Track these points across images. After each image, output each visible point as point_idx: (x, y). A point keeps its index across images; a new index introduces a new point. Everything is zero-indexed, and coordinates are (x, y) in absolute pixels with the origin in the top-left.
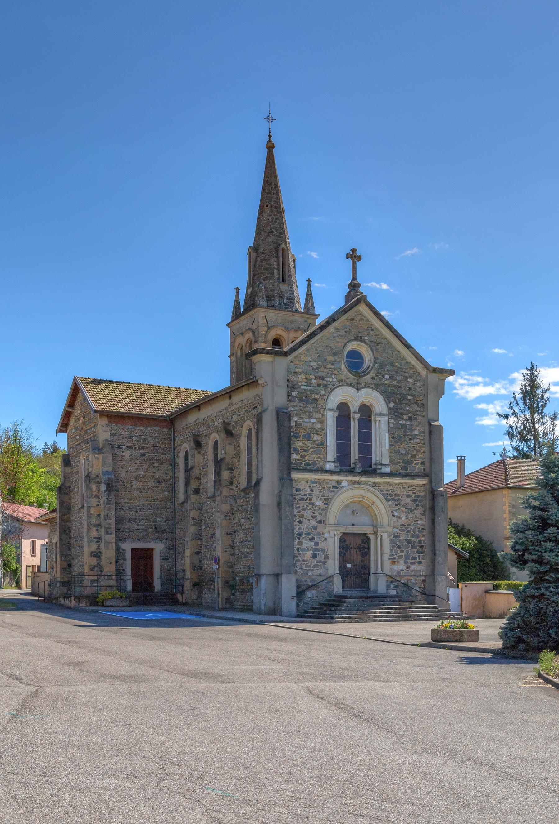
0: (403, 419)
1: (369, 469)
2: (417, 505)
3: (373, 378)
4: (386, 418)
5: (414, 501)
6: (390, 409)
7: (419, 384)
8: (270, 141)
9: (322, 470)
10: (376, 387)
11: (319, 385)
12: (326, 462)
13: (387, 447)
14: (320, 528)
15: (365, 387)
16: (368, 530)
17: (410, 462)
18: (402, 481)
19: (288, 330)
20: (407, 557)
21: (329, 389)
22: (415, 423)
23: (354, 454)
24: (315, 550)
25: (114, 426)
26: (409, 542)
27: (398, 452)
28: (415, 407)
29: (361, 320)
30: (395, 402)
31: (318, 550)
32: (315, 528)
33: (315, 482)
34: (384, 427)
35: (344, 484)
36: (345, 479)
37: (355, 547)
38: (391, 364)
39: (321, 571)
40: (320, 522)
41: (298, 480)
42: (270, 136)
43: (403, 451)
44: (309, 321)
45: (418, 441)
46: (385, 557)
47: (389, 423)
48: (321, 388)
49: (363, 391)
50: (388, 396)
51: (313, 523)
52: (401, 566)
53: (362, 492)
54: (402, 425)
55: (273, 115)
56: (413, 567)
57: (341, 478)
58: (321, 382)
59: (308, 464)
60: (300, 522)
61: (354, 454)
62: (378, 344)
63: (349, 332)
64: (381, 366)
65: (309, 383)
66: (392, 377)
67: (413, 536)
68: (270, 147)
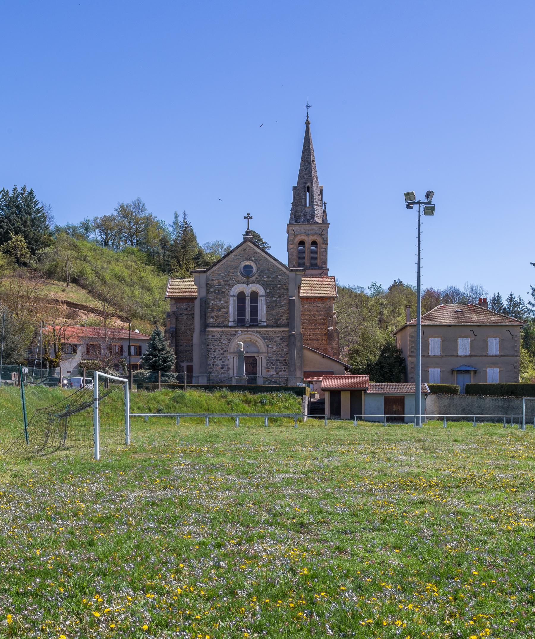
0: (275, 297)
1: (255, 323)
2: (283, 341)
3: (257, 278)
4: (265, 298)
5: (281, 339)
6: (266, 293)
7: (286, 278)
8: (307, 120)
9: (227, 326)
10: (259, 282)
11: (226, 285)
12: (229, 322)
13: (265, 312)
14: (225, 354)
15: (252, 283)
16: (255, 355)
17: (279, 319)
18: (273, 329)
19: (308, 235)
20: (277, 368)
21: (231, 286)
22: (282, 299)
23: (248, 317)
24: (222, 365)
25: (178, 304)
26: (278, 360)
27: (272, 314)
28: (283, 291)
29: (250, 249)
30: (270, 289)
31: (224, 365)
32: (223, 354)
33: (222, 332)
34: (264, 302)
35: (239, 332)
36: (239, 330)
37: (252, 363)
38: (268, 270)
39: (225, 375)
40: (225, 351)
41: (213, 332)
42: (308, 117)
43: (275, 314)
44: (323, 228)
45: (284, 308)
46: (263, 368)
47: (266, 300)
48: (227, 286)
49: (251, 285)
50: (265, 287)
51: (222, 352)
52: (273, 372)
53: (250, 336)
54: (275, 301)
55: (310, 104)
56: (280, 373)
57: (237, 329)
58: (226, 283)
59: (219, 324)
60: (214, 352)
61: (248, 317)
62: (260, 260)
63: (243, 256)
64: (262, 272)
65: (220, 284)
66: (268, 277)
67: (281, 357)
68: (308, 123)
